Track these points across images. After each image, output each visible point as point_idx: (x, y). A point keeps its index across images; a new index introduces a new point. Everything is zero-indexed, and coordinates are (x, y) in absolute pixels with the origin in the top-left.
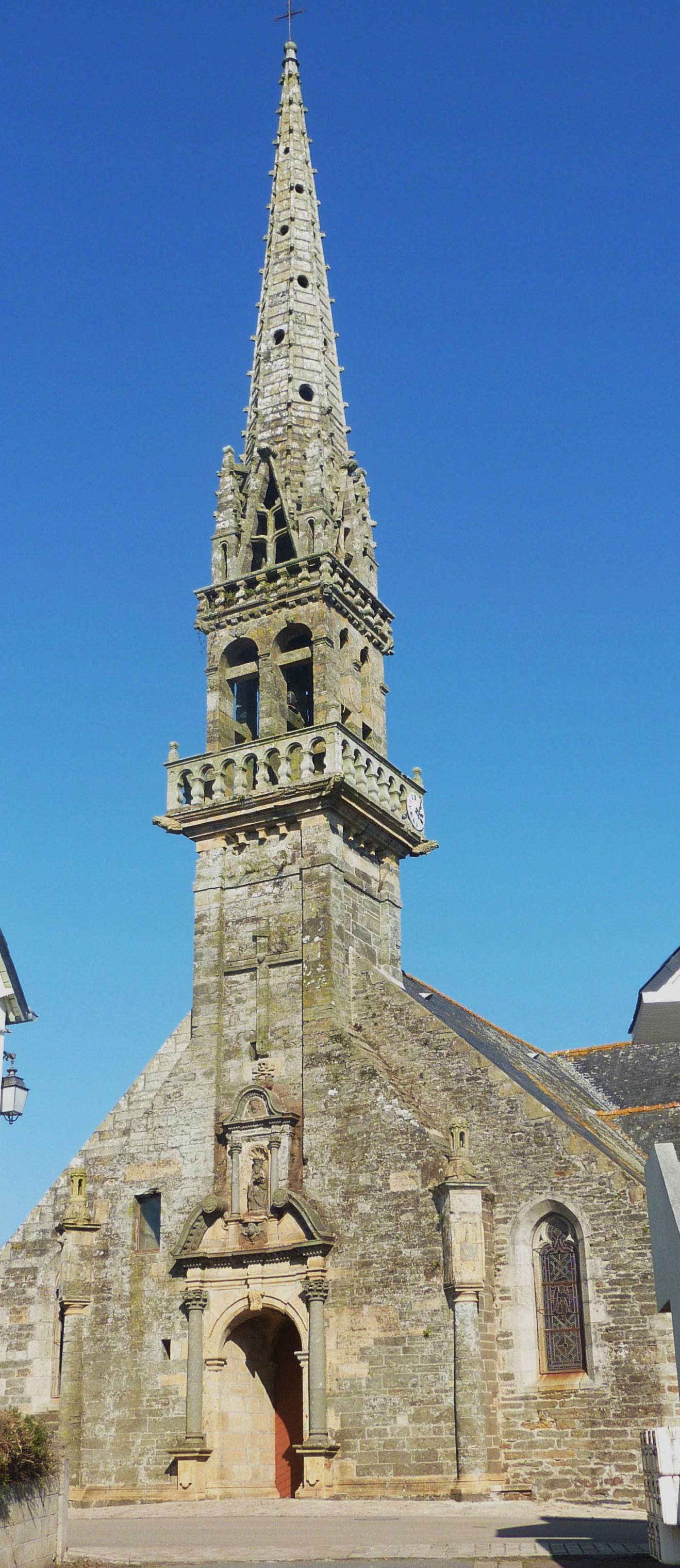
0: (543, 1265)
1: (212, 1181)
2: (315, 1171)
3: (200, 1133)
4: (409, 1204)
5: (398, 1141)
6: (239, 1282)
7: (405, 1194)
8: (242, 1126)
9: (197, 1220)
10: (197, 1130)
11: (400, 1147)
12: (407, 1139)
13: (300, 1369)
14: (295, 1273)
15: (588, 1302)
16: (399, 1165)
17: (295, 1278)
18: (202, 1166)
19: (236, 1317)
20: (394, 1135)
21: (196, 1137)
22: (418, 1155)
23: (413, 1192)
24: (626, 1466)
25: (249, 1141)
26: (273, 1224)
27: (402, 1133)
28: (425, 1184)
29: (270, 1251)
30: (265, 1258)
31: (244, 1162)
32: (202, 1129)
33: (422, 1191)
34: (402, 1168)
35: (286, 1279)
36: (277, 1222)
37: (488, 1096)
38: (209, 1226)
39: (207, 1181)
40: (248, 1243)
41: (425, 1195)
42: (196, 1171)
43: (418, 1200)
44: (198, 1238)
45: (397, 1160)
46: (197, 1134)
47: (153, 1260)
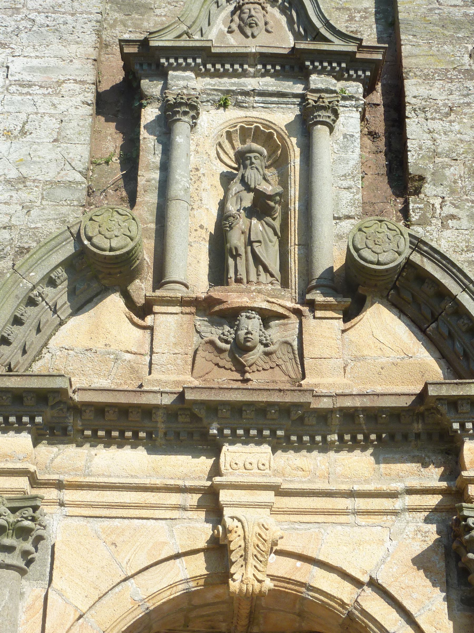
1: (81, 194)
2: (449, 210)
3: (45, 70)
6: (175, 499)
8: (208, 59)
9: (52, 283)
10: (35, 62)
14: (399, 486)
15: (185, 486)
17: (398, 504)
18: (46, 152)
19: (149, 614)
21: (27, 77)
25: (225, 105)
26: (324, 332)
29: (325, 403)
30: (295, 423)
31: (202, 153)
32: (53, 62)
35: (362, 504)
36: (339, 324)
38: (78, 308)
39: (60, 193)
40: (226, 377)
42: (19, 163)
44: (35, 340)
46: (32, 69)
47: (292, 302)
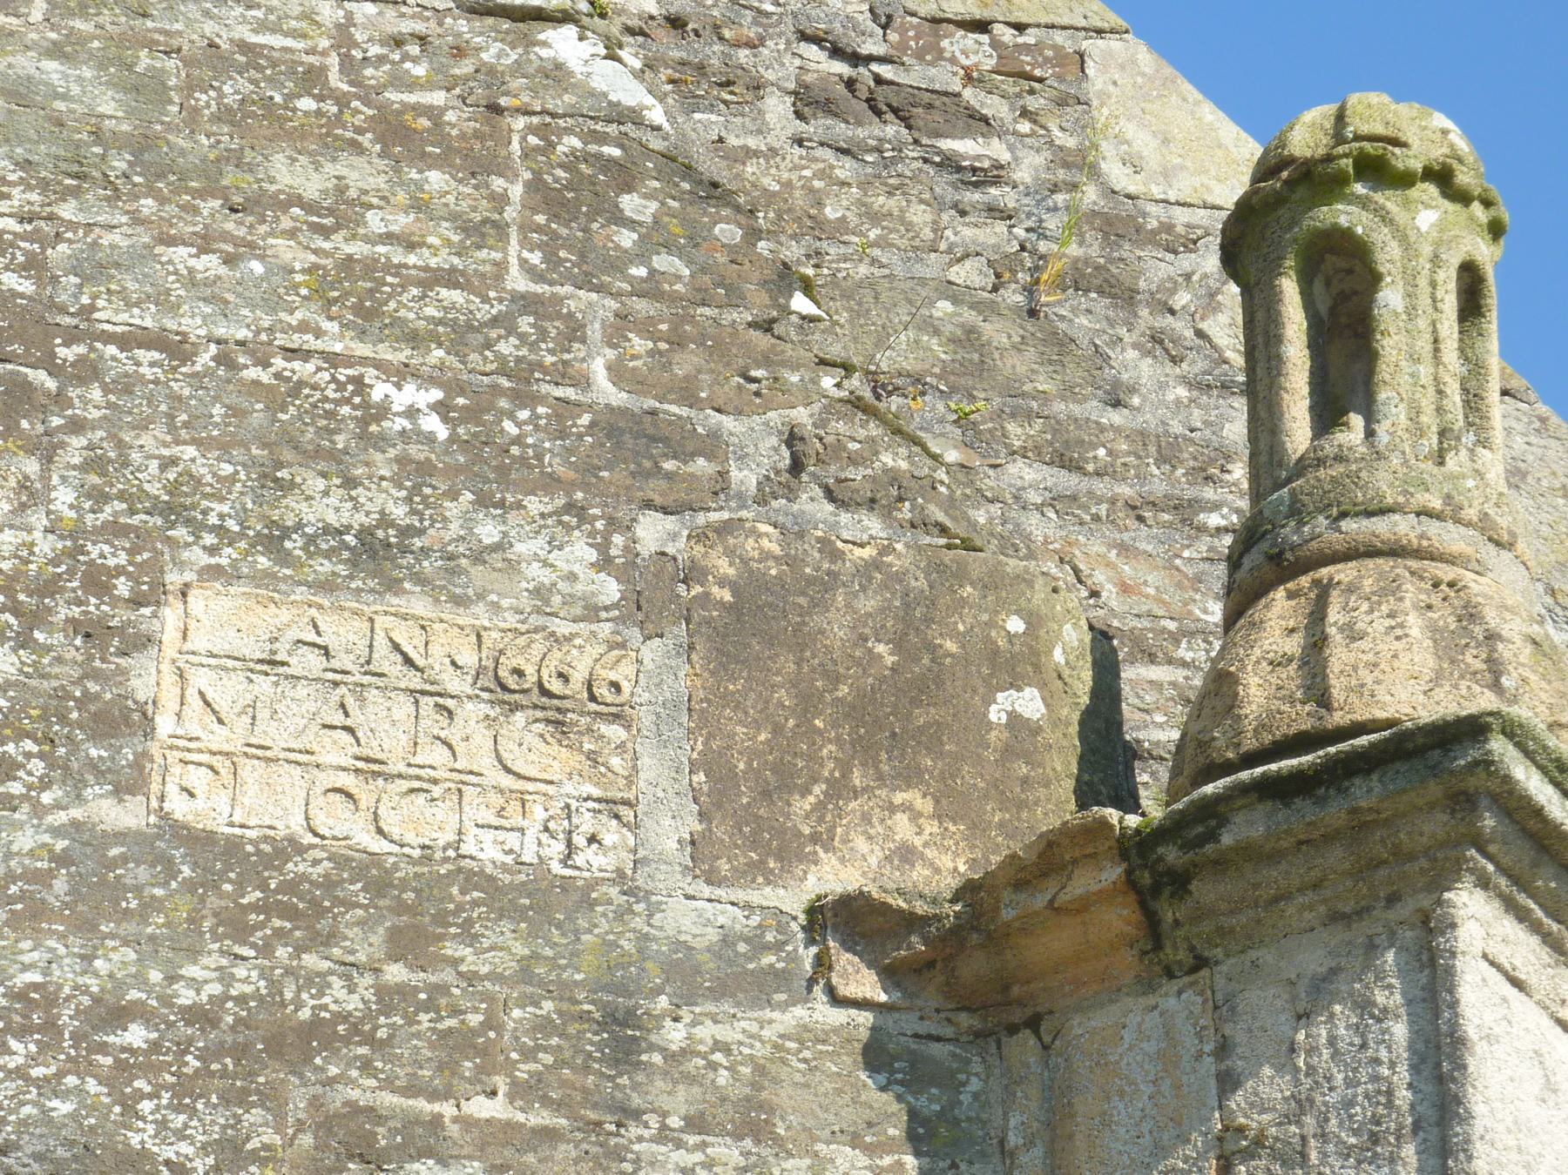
0: (1279, 339)
4: (467, 1054)
5: (341, 212)
7: (421, 904)
11: (358, 293)
12: (482, 231)
13: (1398, 99)
16: (319, 504)
20: (261, 122)
22: (640, 453)
23: (539, 899)
24: (1541, 924)
27: (399, 136)
28: (745, 819)
33: (693, 915)
34: (376, 556)
37: (1082, 318)
41: (735, 976)
43: (623, 1035)
45: (312, 432)
